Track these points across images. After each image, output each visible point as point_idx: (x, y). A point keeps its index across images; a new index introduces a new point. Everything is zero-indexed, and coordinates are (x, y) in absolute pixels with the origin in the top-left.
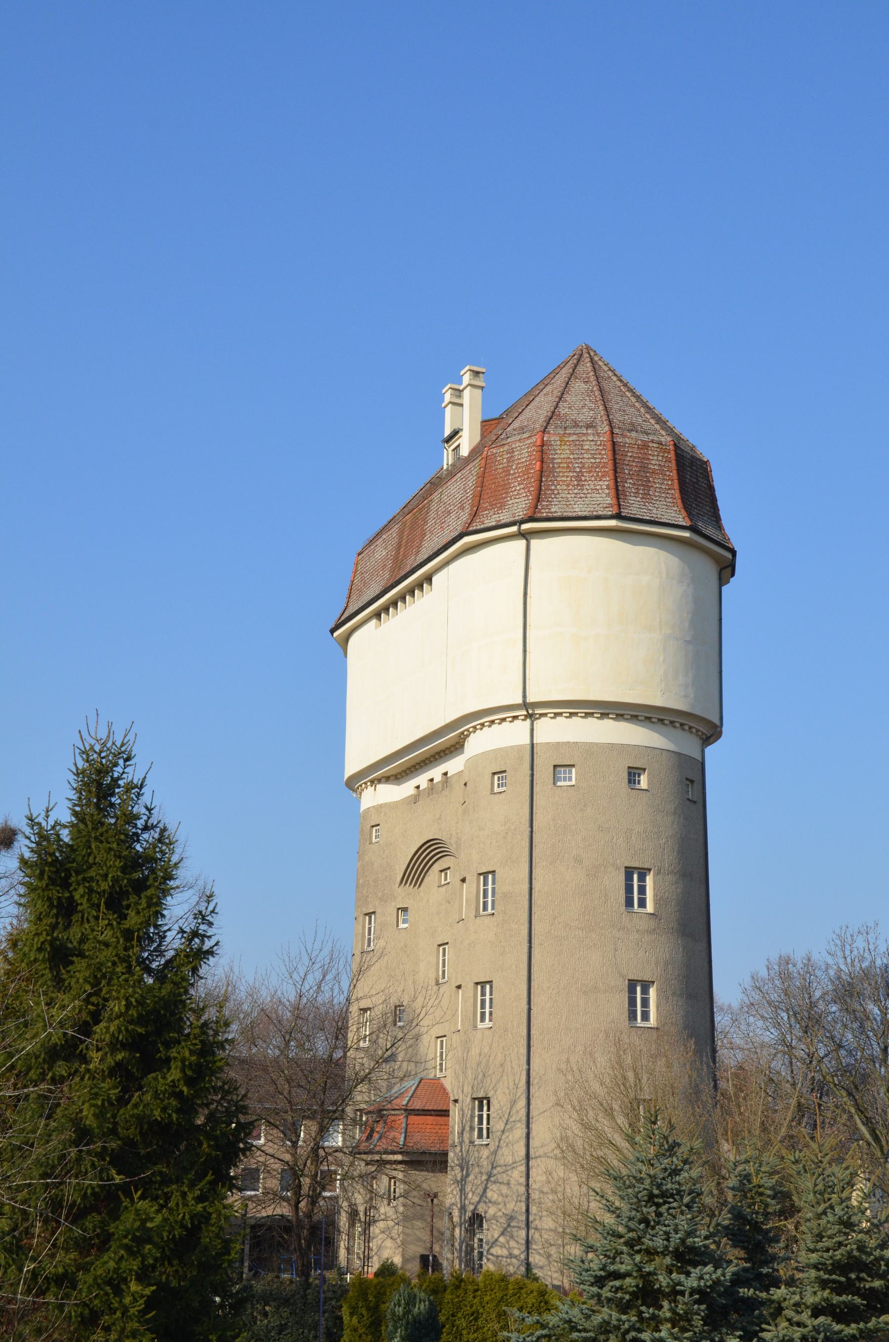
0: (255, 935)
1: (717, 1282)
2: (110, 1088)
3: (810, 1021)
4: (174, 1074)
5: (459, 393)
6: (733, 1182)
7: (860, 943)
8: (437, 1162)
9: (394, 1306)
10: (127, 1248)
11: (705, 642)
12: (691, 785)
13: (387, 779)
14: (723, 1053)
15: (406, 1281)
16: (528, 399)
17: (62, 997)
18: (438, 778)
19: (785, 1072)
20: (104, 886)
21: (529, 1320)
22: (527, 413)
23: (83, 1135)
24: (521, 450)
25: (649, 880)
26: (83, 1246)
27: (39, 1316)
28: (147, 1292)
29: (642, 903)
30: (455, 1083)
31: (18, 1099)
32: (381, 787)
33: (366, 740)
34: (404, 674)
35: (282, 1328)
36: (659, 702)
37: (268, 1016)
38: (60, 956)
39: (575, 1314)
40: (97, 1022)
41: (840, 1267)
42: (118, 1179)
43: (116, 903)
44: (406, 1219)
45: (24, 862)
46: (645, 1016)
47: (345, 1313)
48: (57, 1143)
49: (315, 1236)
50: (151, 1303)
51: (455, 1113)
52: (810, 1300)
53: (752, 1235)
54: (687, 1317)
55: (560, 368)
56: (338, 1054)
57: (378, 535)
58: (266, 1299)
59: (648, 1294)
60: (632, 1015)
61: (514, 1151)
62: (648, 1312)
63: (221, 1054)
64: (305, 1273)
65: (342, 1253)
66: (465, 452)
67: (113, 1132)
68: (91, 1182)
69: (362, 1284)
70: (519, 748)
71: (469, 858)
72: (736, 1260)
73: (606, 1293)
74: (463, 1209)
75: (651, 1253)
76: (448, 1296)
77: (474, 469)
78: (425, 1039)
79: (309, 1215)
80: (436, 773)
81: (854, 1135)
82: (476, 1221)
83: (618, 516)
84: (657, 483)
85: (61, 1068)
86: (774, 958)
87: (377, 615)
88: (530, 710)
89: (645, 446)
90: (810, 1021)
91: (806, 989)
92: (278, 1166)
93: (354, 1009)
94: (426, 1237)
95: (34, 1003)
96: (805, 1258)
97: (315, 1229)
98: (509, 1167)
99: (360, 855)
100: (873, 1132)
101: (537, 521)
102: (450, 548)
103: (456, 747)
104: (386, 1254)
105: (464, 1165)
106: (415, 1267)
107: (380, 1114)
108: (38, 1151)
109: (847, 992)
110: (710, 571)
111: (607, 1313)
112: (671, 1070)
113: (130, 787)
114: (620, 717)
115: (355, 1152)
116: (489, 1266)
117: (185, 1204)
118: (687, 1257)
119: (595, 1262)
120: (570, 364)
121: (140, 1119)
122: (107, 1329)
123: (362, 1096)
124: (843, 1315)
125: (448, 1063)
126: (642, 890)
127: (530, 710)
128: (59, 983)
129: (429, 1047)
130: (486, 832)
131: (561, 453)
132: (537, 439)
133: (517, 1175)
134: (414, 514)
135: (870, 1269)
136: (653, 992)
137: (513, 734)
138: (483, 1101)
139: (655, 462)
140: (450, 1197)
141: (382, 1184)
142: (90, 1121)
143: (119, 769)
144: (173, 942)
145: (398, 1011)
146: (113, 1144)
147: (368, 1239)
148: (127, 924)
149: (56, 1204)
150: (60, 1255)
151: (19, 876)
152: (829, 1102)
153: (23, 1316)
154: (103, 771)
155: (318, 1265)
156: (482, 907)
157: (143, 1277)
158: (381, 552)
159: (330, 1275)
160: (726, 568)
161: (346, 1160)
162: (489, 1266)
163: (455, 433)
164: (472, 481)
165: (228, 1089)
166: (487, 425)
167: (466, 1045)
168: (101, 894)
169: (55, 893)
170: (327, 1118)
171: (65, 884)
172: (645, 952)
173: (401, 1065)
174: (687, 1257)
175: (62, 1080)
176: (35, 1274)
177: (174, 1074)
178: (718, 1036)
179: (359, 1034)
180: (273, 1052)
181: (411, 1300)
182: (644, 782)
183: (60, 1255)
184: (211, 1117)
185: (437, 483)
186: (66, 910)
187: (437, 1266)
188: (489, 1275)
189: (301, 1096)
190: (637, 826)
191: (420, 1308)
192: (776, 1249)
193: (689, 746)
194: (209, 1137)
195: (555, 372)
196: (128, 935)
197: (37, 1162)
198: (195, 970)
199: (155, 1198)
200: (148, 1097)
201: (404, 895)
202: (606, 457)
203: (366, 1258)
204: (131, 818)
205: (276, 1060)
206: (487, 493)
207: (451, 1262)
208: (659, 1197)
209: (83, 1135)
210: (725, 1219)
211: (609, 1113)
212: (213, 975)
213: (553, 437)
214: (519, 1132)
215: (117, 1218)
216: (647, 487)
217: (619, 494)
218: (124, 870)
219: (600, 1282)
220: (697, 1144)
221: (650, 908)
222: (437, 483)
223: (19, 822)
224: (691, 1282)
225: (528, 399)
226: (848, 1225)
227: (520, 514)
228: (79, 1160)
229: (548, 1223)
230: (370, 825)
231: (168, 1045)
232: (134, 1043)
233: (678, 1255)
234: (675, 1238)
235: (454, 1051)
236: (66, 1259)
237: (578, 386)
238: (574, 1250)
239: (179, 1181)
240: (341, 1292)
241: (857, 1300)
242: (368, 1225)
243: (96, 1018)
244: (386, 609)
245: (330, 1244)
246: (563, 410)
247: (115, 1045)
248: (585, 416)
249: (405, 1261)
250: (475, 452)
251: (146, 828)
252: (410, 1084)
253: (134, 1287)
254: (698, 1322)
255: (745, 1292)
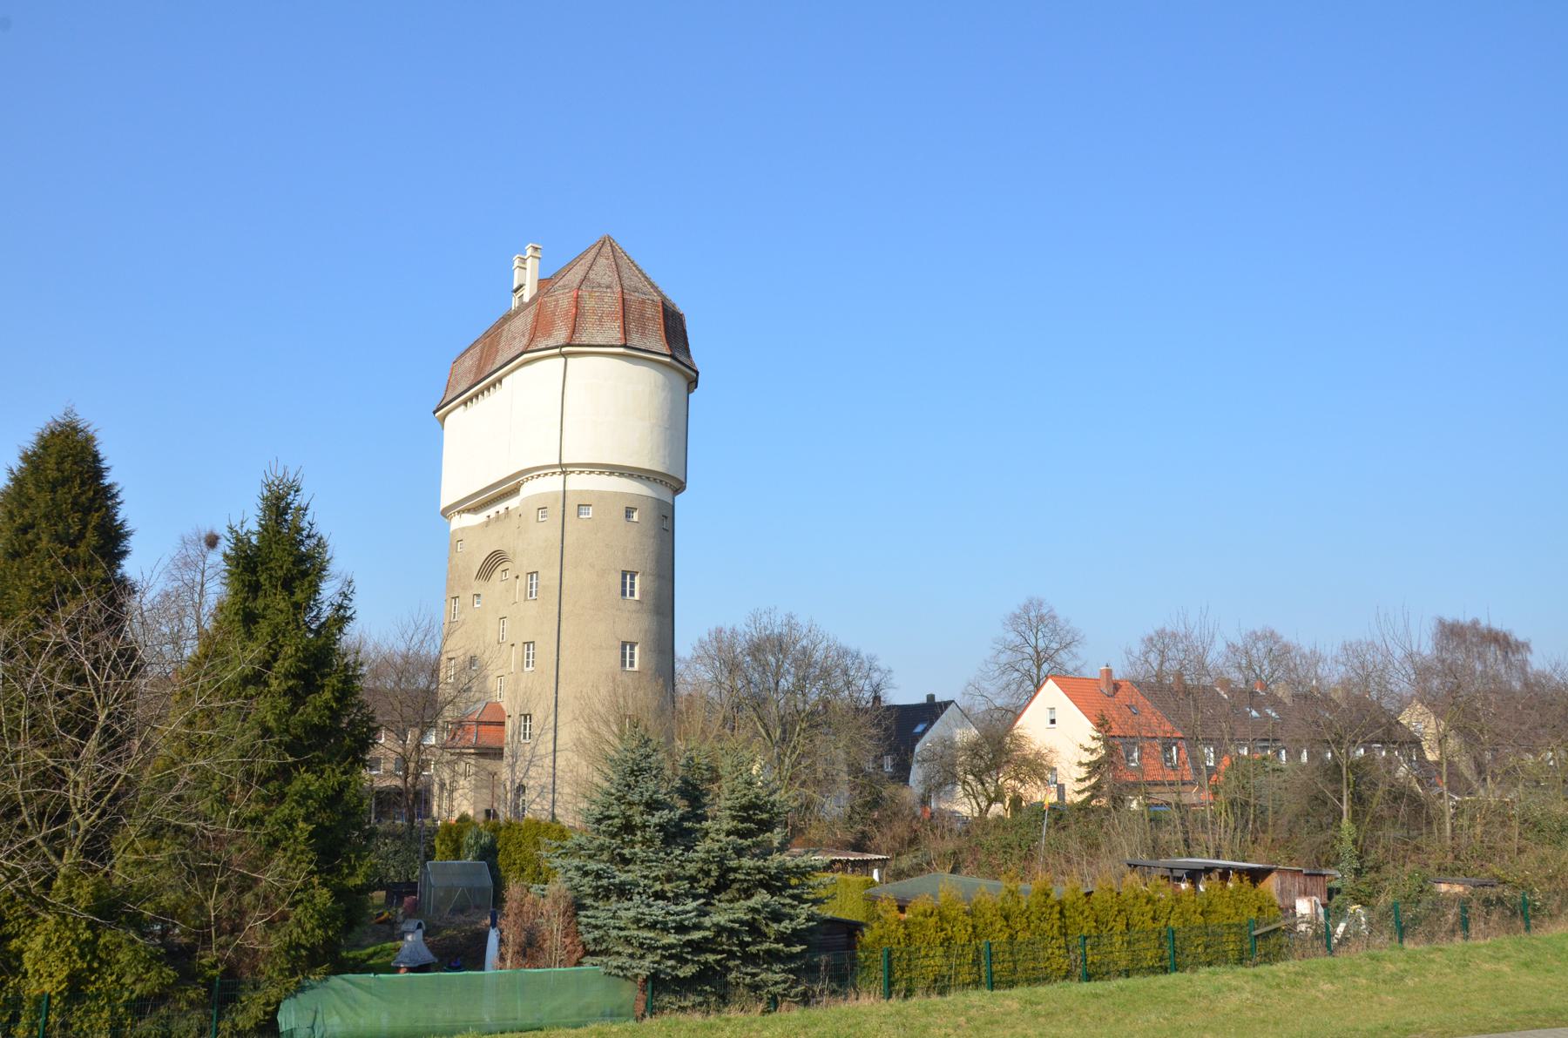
0: (380, 609)
1: (671, 820)
2: (284, 704)
3: (733, 667)
4: (327, 695)
5: (524, 261)
6: (683, 761)
7: (765, 619)
8: (497, 753)
9: (468, 838)
10: (297, 802)
11: (677, 430)
12: (665, 520)
13: (468, 510)
14: (679, 687)
15: (475, 824)
16: (569, 267)
17: (251, 645)
18: (502, 511)
19: (717, 698)
20: (280, 573)
21: (555, 844)
22: (569, 276)
23: (266, 732)
24: (565, 301)
25: (637, 579)
26: (268, 800)
27: (240, 841)
28: (310, 828)
29: (632, 594)
30: (509, 705)
31: (222, 708)
32: (465, 516)
33: (454, 488)
34: (481, 442)
35: (396, 852)
36: (647, 466)
37: (388, 662)
38: (250, 619)
39: (583, 840)
40: (276, 660)
41: (744, 808)
42: (290, 760)
43: (288, 585)
44: (476, 788)
45: (226, 556)
46: (632, 664)
47: (437, 843)
48: (248, 736)
49: (419, 799)
50: (312, 835)
51: (509, 723)
52: (725, 827)
53: (693, 794)
54: (651, 840)
55: (587, 251)
56: (433, 686)
57: (467, 350)
58: (386, 835)
59: (628, 827)
60: (623, 663)
61: (545, 747)
62: (627, 838)
63: (357, 683)
64: (411, 820)
65: (435, 808)
66: (526, 299)
67: (287, 730)
68: (273, 761)
69: (449, 829)
70: (555, 493)
71: (522, 562)
72: (682, 806)
73: (603, 828)
74: (513, 781)
75: (631, 804)
76: (503, 833)
77: (533, 309)
78: (491, 679)
79: (414, 786)
80: (501, 507)
81: (757, 733)
82: (521, 789)
83: (625, 346)
84: (650, 325)
85: (251, 690)
86: (713, 628)
87: (465, 403)
88: (564, 469)
89: (643, 302)
90: (733, 667)
91: (732, 646)
92: (394, 756)
93: (444, 658)
94: (489, 798)
95: (233, 648)
96: (723, 803)
97: (417, 794)
98: (542, 757)
99: (450, 560)
100: (767, 732)
101: (572, 347)
102: (528, 352)
103: (514, 491)
104: (463, 809)
105: (514, 756)
106: (482, 817)
107: (460, 724)
108: (238, 741)
109: (756, 649)
110: (682, 384)
111: (606, 840)
112: (645, 698)
113: (299, 509)
114: (621, 475)
115: (443, 747)
116: (528, 815)
117: (334, 776)
118: (652, 806)
119: (596, 810)
120: (594, 252)
121: (304, 724)
122: (285, 849)
123: (449, 713)
124: (742, 834)
125: (506, 694)
126: (632, 585)
127: (564, 469)
128: (250, 636)
129: (493, 683)
130: (533, 546)
131: (589, 304)
132: (573, 294)
133: (548, 761)
134: (491, 339)
135: (761, 808)
136: (637, 649)
137: (553, 484)
138: (527, 717)
139: (649, 312)
140: (505, 774)
141: (461, 767)
142: (272, 724)
143: (290, 498)
144: (327, 612)
145: (472, 661)
146: (287, 738)
147: (451, 799)
148: (294, 599)
149: (249, 774)
150: (253, 805)
151: (223, 565)
152: (743, 715)
153: (231, 841)
154: (280, 498)
155: (419, 815)
156: (529, 594)
157: (307, 819)
158: (469, 362)
159: (428, 822)
160: (692, 383)
161: (438, 752)
162: (528, 815)
163: (521, 286)
164: (530, 319)
165: (361, 706)
166: (542, 283)
167: (517, 681)
168: (278, 579)
169: (246, 577)
170: (426, 727)
171: (254, 571)
172: (634, 624)
173: (475, 694)
174: (652, 806)
175: (252, 697)
176: (237, 816)
177: (327, 695)
178: (677, 677)
179: (447, 674)
180: (390, 684)
181: (479, 836)
182: (636, 516)
183: (253, 805)
184: (351, 722)
185: (507, 318)
186: (254, 588)
187: (496, 815)
188: (529, 821)
189: (408, 712)
190: (628, 545)
191: (485, 840)
192: (706, 800)
193: (665, 495)
194: (350, 735)
195: (587, 251)
196: (297, 606)
197: (237, 749)
198: (340, 630)
199: (314, 772)
200: (310, 709)
201: (478, 587)
202: (619, 308)
203: (451, 811)
204: (299, 530)
205: (392, 690)
206: (540, 327)
207: (504, 813)
208: (638, 771)
209: (266, 732)
210: (678, 783)
211: (607, 723)
212: (351, 635)
213: (584, 293)
214: (551, 735)
215: (290, 783)
216: (644, 328)
217: (625, 332)
218: (294, 563)
219: (599, 821)
220: (662, 740)
221: (637, 597)
222: (507, 318)
223: (222, 530)
224: (655, 820)
225: (569, 267)
226: (750, 783)
227: (562, 342)
228: (264, 747)
229: (567, 790)
230: (456, 541)
231: (323, 676)
232: (301, 675)
233: (647, 805)
234: (646, 795)
235: (509, 685)
236: (255, 808)
237: (602, 261)
238: (584, 805)
239: (330, 761)
240: (434, 831)
241: (707, 933)
242: (451, 792)
243: (275, 658)
244: (471, 399)
245: (427, 803)
246: (592, 275)
247: (287, 676)
248: (606, 280)
249: (476, 813)
250: (533, 300)
251: (308, 537)
252: (480, 706)
253: (301, 825)
254: (658, 843)
255: (687, 824)
